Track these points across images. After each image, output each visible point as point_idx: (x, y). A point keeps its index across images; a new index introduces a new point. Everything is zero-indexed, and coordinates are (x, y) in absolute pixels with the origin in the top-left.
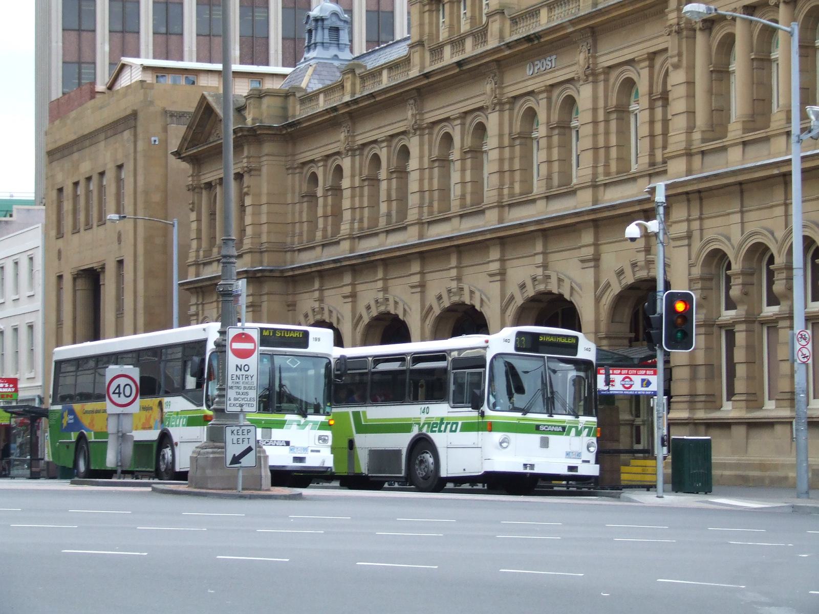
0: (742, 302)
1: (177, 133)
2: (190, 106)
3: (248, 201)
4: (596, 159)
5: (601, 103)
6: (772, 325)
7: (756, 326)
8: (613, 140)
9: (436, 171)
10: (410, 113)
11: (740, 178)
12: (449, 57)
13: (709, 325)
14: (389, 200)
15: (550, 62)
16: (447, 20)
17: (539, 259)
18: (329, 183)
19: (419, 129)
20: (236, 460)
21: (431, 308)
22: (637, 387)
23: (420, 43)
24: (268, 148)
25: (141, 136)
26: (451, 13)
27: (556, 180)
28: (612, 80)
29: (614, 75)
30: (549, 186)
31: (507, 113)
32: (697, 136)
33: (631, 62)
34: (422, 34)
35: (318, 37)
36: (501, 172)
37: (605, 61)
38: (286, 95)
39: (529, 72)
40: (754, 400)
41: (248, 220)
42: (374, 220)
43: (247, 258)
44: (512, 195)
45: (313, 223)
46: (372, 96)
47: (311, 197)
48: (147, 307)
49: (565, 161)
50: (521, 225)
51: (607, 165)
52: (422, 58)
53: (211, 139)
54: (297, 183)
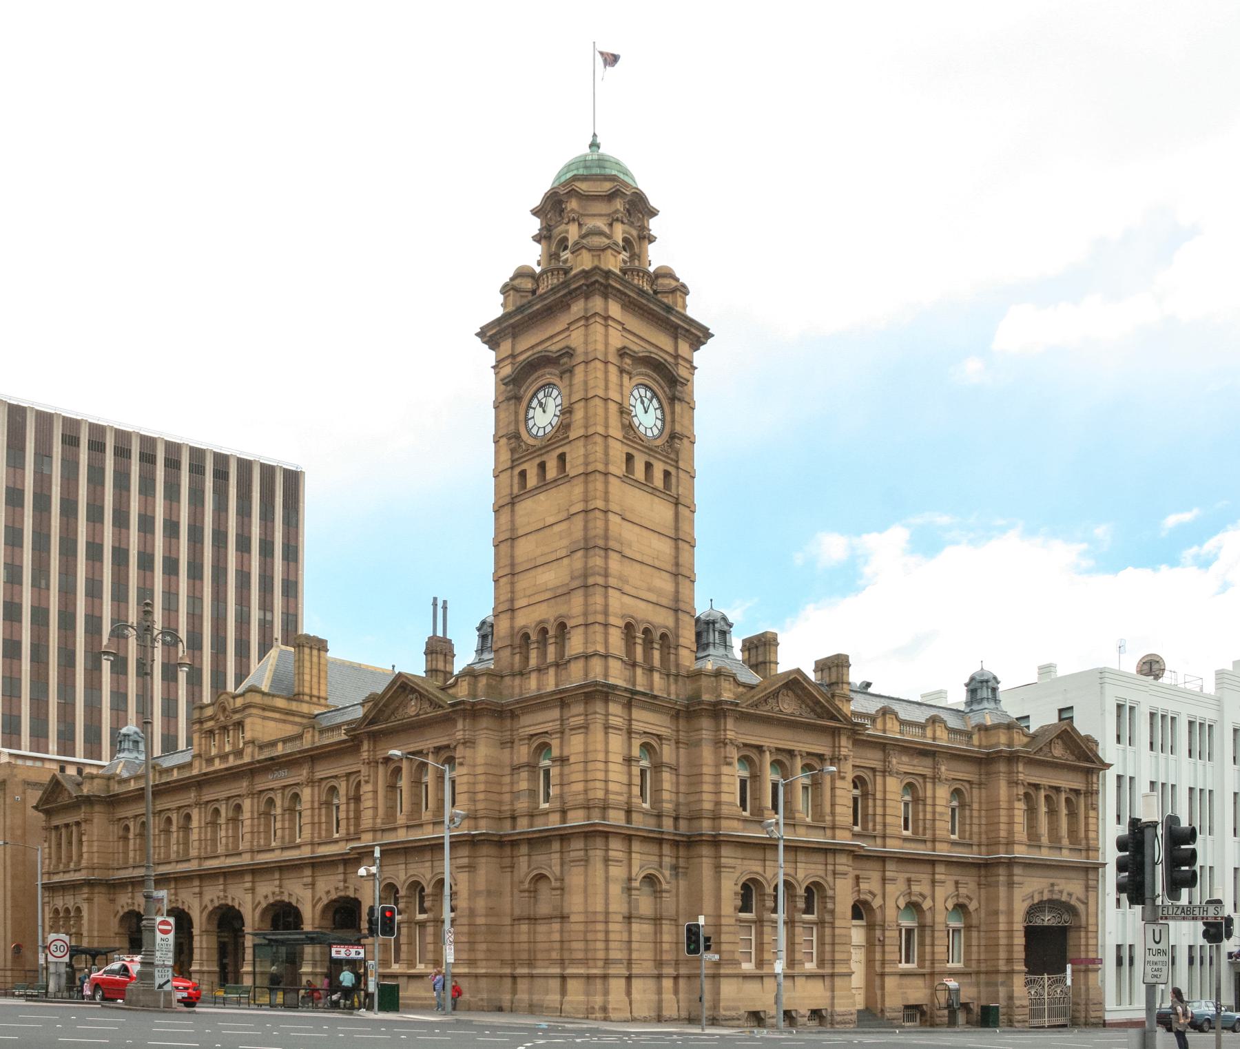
0: (405, 912)
1: (34, 796)
2: (46, 779)
3: (84, 838)
4: (313, 829)
5: (316, 799)
6: (422, 924)
7: (413, 925)
8: (323, 819)
9: (209, 829)
10: (193, 795)
11: (406, 845)
12: (218, 765)
13: (411, 922)
14: (178, 843)
15: (283, 773)
16: (217, 743)
17: (277, 882)
18: (137, 831)
19: (198, 804)
20: (160, 986)
21: (206, 906)
22: (353, 955)
23: (199, 755)
24: (97, 808)
25: (8, 795)
26: (234, 736)
27: (287, 838)
28: (323, 786)
29: (324, 784)
30: (227, 850)
31: (256, 800)
32: (379, 821)
33: (336, 777)
34: (200, 749)
35: (126, 745)
36: (252, 832)
37: (319, 775)
38: (109, 778)
39: (270, 777)
40: (411, 964)
41: (85, 849)
42: (168, 854)
43: (84, 872)
44: (259, 845)
45: (126, 853)
46: (168, 783)
47: (126, 839)
48: (13, 896)
49: (236, 837)
50: (266, 863)
51: (320, 833)
52: (201, 765)
53: (59, 800)
54: (116, 830)
